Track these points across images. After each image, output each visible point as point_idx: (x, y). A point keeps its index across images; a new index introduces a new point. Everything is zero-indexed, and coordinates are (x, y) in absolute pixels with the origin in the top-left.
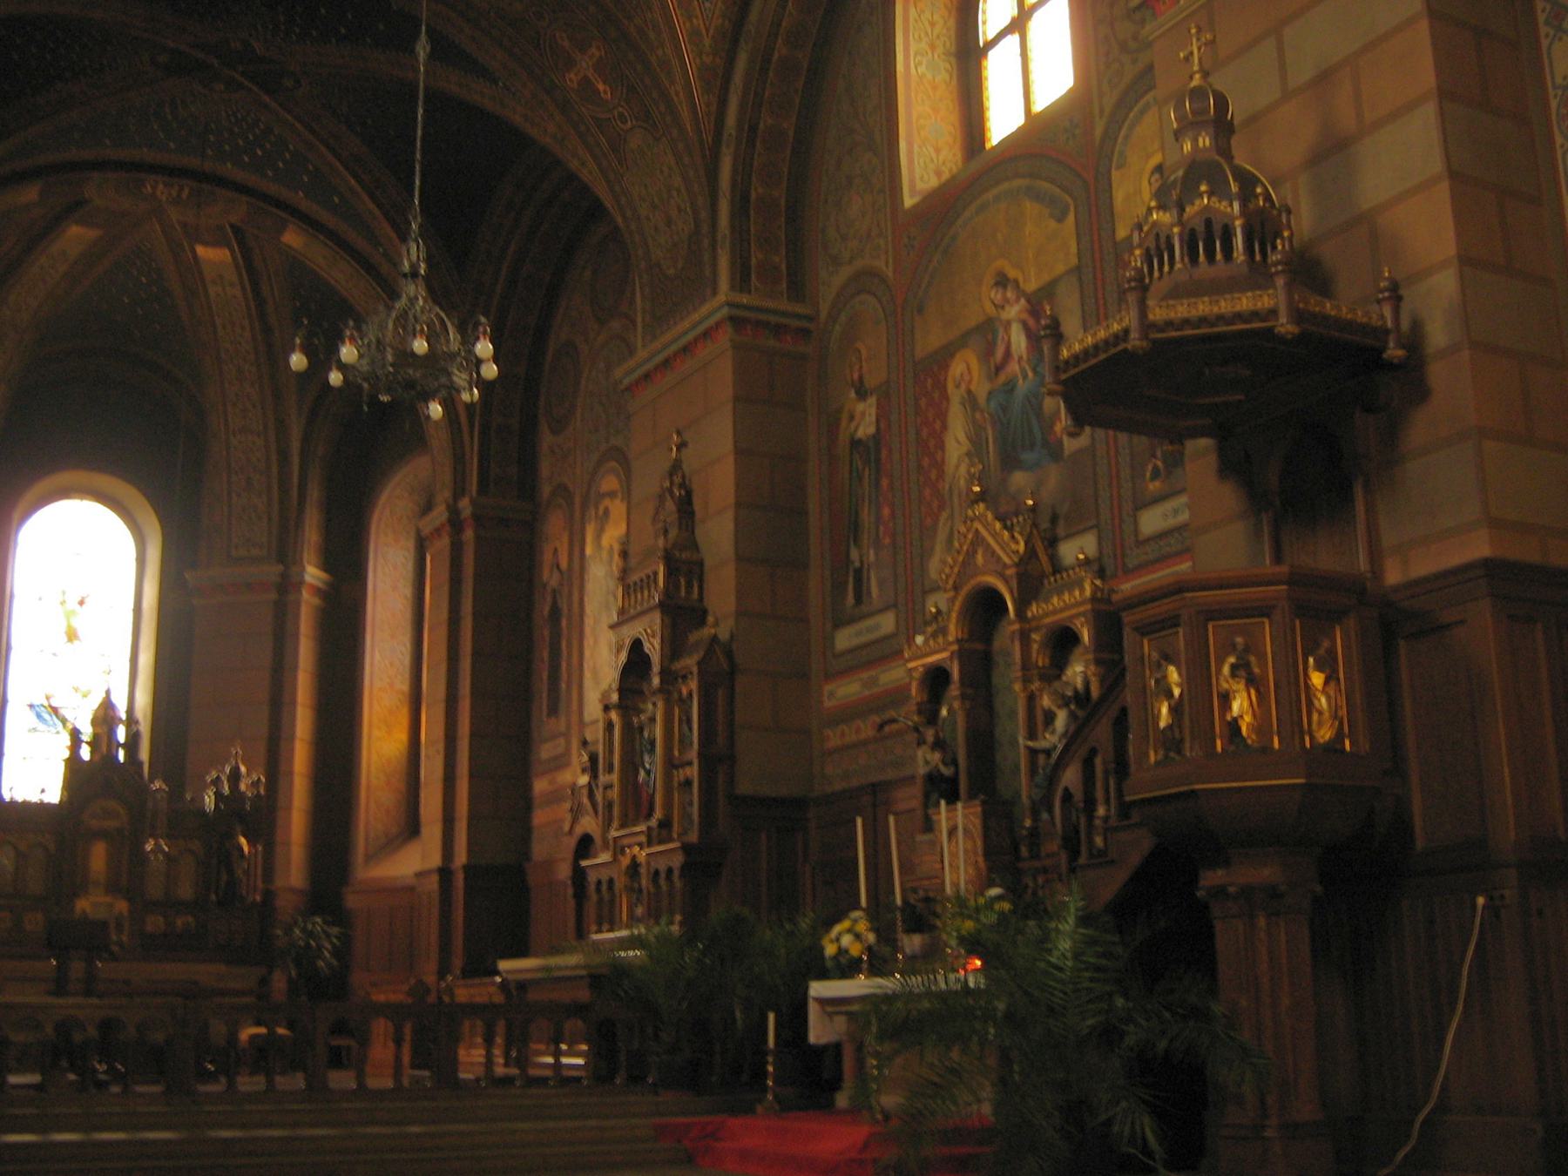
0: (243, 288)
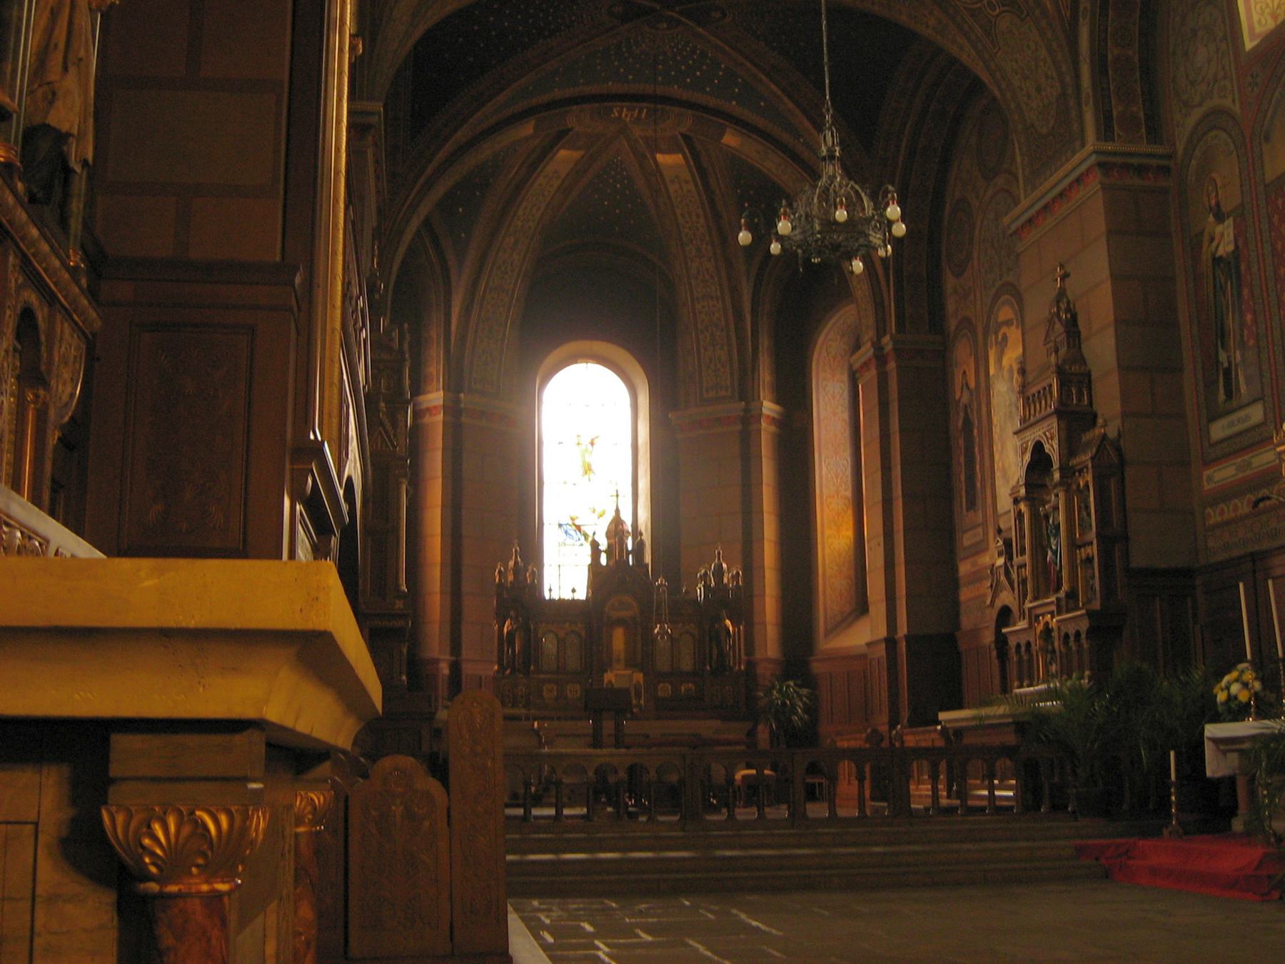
0: (696, 185)
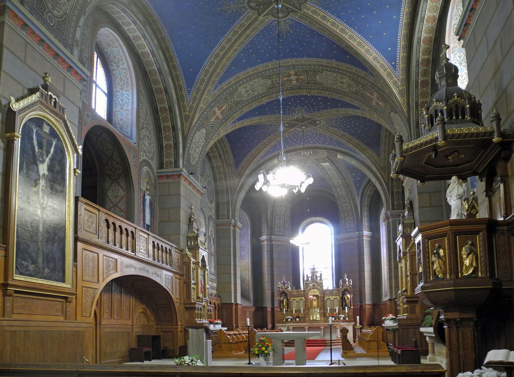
0: (335, 170)
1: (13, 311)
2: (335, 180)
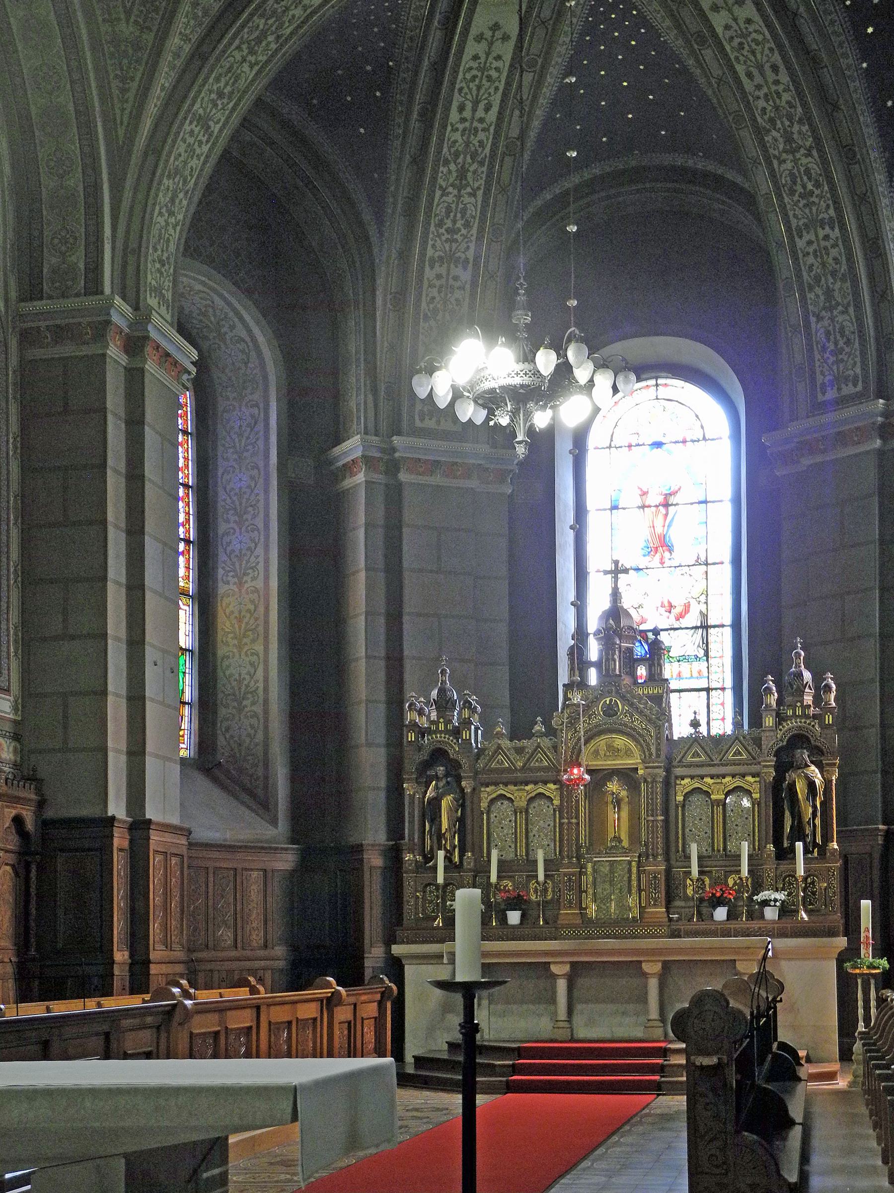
1: (265, 876)
2: (758, 79)
